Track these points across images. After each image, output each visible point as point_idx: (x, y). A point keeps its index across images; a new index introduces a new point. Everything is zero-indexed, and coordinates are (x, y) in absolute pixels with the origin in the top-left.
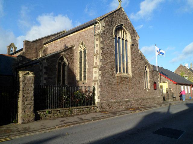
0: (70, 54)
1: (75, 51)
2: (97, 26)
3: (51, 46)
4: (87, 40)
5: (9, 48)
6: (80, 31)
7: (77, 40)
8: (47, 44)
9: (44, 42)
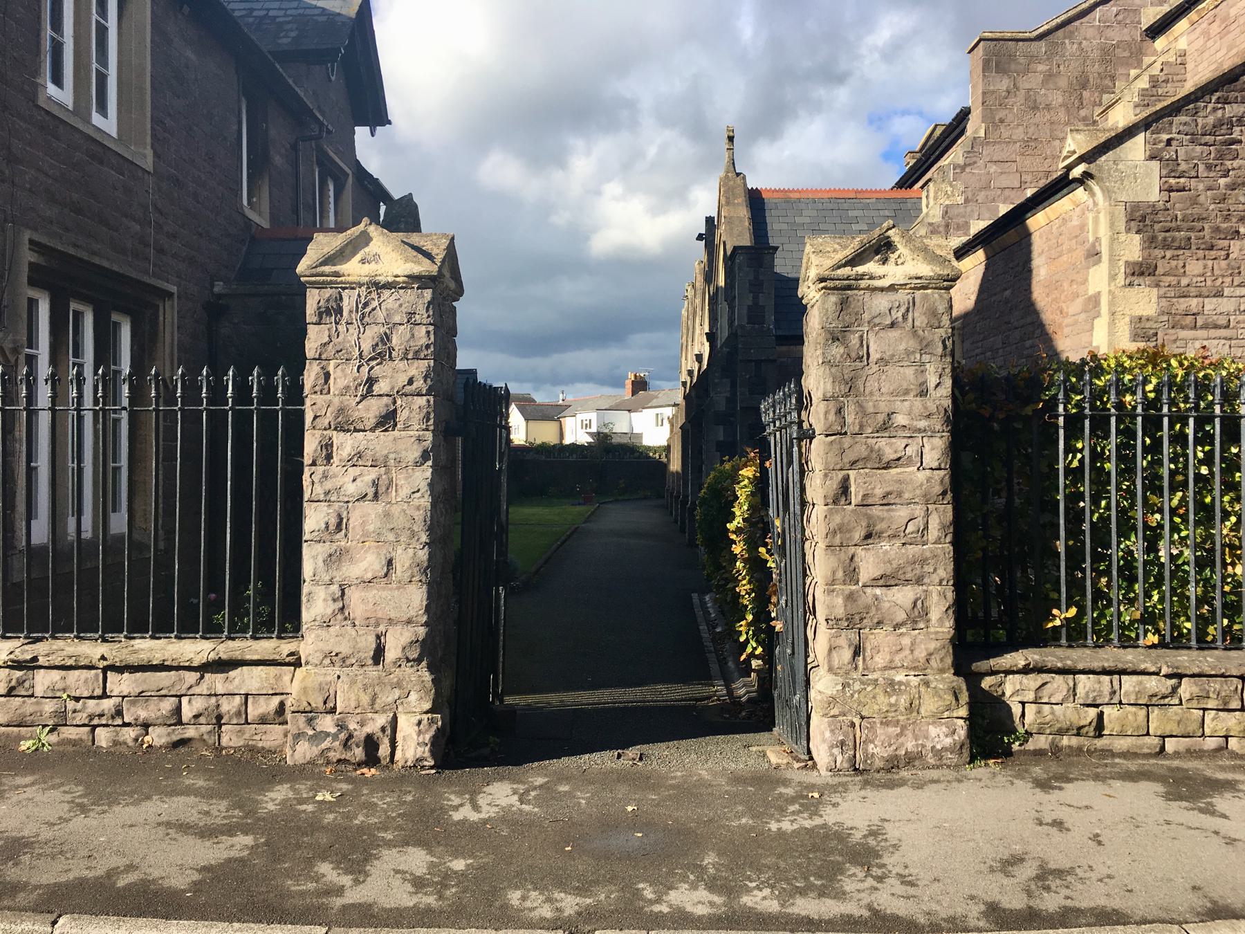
3: (1215, 28)
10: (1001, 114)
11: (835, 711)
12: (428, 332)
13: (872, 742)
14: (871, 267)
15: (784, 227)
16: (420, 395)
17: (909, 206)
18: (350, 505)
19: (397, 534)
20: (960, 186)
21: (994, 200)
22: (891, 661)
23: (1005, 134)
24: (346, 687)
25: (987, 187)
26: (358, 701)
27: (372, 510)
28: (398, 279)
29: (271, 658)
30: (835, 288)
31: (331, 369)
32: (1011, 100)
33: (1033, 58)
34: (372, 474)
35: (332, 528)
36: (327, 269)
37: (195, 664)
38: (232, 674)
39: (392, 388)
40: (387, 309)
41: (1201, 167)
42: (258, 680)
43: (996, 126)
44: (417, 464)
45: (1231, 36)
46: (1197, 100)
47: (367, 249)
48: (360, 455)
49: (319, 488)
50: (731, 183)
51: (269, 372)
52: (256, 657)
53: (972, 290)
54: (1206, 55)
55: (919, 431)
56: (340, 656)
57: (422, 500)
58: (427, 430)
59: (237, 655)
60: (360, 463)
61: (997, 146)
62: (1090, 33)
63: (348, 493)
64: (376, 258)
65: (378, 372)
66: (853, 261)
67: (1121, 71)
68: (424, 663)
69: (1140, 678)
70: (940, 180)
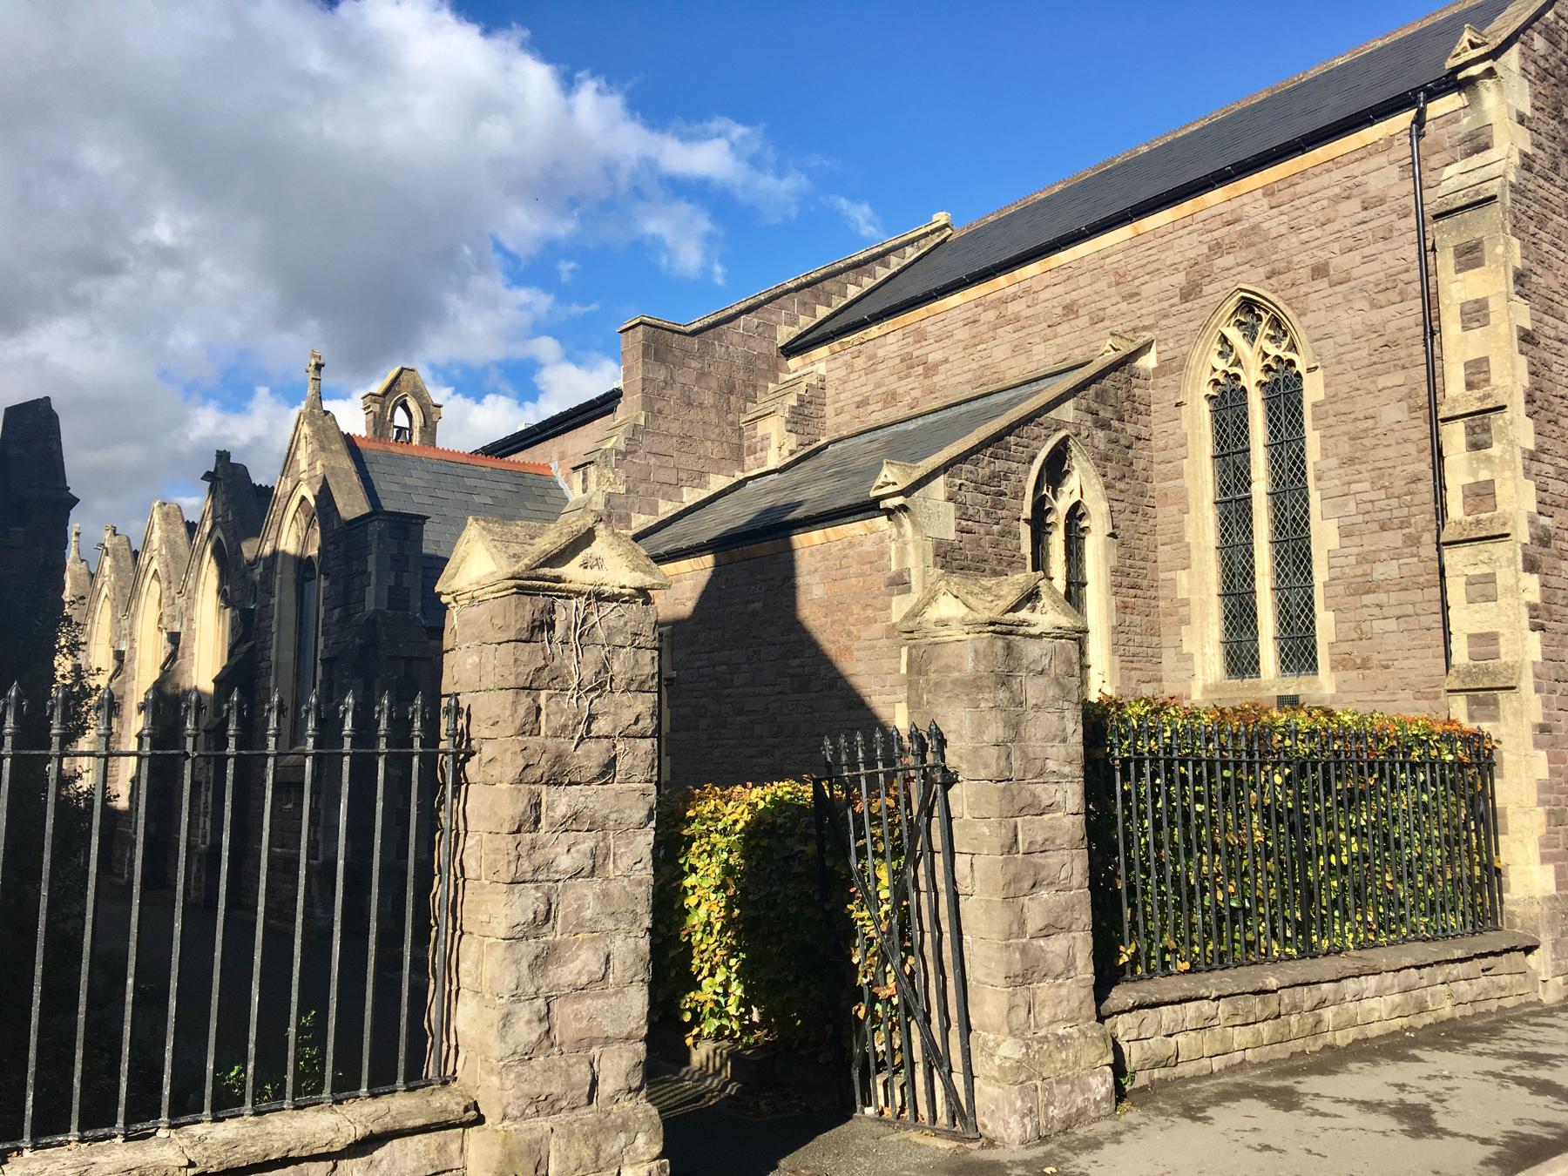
0: (1121, 420)
1: (1159, 395)
2: (1451, 118)
3: (860, 363)
4: (1319, 271)
5: (383, 408)
6: (1214, 197)
7: (1180, 279)
8: (822, 351)
9: (785, 334)
10: (659, 405)
11: (1023, 1077)
12: (653, 658)
13: (1052, 1104)
14: (1024, 614)
15: (395, 488)
16: (643, 737)
17: (529, 482)
18: (560, 884)
19: (617, 920)
20: (622, 473)
21: (653, 494)
22: (1055, 1014)
23: (663, 427)
24: (562, 1142)
25: (646, 480)
26: (580, 1159)
27: (588, 890)
28: (623, 591)
29: (442, 1119)
30: (1001, 633)
31: (542, 701)
32: (668, 392)
33: (687, 353)
34: (588, 842)
35: (540, 918)
36: (546, 571)
37: (337, 1147)
38: (378, 1154)
39: (614, 729)
40: (609, 627)
41: (982, 513)
42: (415, 1156)
43: (655, 417)
44: (642, 826)
45: (879, 375)
46: (977, 452)
47: (588, 551)
48: (576, 816)
49: (527, 864)
50: (320, 422)
51: (402, 700)
52: (420, 1122)
53: (688, 594)
54: (850, 385)
55: (1065, 776)
56: (550, 1099)
57: (644, 872)
58: (650, 781)
59: (389, 1123)
60: (574, 827)
61: (656, 438)
62: (736, 339)
63: (561, 868)
64: (598, 563)
65: (599, 707)
66: (1015, 608)
67: (761, 382)
68: (643, 1093)
69: (1197, 1003)
70: (602, 465)
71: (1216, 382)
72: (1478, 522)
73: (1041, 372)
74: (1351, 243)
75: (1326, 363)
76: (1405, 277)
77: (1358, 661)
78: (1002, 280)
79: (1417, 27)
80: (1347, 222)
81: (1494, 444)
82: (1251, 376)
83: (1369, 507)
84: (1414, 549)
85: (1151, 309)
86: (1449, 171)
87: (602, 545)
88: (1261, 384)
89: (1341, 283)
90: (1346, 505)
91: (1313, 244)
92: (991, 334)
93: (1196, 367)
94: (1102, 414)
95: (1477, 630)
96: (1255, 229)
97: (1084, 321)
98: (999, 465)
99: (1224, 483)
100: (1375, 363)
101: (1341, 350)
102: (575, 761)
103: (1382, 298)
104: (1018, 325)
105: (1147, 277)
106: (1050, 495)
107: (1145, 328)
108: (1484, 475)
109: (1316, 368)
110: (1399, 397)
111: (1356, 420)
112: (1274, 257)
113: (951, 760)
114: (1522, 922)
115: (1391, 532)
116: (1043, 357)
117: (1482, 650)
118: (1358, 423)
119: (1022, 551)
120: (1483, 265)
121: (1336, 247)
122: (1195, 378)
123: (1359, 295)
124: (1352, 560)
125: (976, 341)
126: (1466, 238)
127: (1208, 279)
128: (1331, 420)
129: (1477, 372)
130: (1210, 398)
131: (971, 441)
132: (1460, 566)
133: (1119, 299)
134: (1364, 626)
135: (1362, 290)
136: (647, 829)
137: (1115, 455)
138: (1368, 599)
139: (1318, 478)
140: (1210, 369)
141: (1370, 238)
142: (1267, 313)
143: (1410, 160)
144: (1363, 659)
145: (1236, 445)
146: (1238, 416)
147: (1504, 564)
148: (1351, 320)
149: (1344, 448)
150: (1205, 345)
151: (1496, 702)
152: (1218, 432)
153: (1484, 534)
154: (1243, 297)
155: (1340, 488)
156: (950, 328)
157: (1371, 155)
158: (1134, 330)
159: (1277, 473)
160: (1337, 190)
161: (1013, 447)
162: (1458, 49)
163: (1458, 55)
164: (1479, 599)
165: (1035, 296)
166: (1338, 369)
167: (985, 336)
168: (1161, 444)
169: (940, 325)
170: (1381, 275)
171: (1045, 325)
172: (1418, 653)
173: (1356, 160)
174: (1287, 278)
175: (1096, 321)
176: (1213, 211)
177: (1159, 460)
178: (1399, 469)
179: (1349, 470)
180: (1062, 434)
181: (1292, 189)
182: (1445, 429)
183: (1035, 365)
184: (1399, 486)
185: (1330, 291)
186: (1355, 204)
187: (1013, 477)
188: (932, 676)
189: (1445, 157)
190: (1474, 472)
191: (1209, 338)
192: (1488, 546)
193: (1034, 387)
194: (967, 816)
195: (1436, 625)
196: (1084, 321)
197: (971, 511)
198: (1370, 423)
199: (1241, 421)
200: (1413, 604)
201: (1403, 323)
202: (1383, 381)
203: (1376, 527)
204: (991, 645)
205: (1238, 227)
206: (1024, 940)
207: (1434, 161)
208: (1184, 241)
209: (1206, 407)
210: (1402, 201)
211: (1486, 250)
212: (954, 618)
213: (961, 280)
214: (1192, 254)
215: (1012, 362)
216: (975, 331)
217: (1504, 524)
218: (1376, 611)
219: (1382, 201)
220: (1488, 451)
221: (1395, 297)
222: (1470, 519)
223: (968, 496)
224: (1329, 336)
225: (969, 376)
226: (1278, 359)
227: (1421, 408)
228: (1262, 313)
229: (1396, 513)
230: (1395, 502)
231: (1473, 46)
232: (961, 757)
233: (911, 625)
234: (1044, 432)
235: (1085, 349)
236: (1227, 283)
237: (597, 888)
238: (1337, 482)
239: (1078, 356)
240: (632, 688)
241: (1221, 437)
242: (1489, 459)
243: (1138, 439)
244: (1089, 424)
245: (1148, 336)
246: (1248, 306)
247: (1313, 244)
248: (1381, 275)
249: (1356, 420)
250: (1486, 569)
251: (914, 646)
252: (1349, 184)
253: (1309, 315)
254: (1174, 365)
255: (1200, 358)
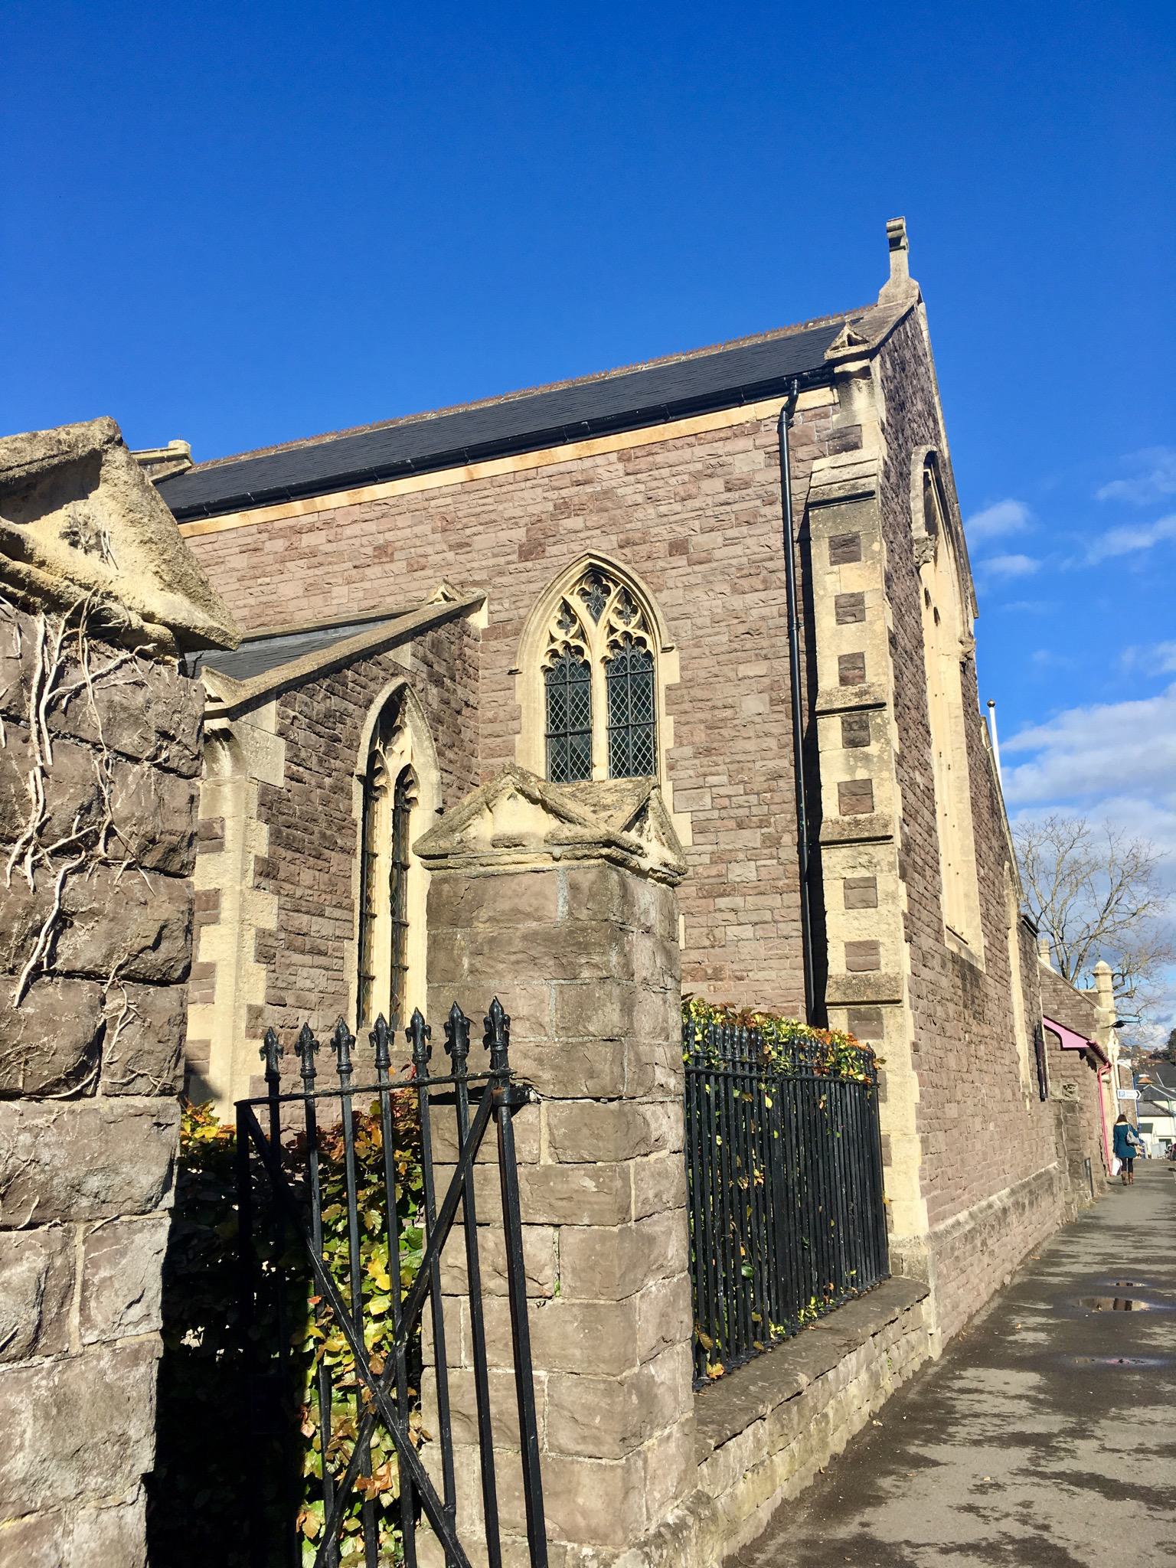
0: (453, 679)
1: (488, 658)
2: (821, 413)
4: (678, 547)
6: (565, 452)
7: (519, 534)
28: (149, 627)
39: (109, 956)
41: (314, 759)
57: (143, 1328)
65: (81, 896)
71: (554, 654)
72: (857, 823)
73: (343, 617)
74: (712, 522)
75: (684, 644)
76: (769, 565)
77: (710, 971)
78: (297, 506)
79: (721, 350)
80: (709, 500)
81: (873, 742)
82: (597, 650)
83: (726, 802)
84: (774, 850)
85: (484, 563)
86: (817, 465)
87: (111, 505)
88: (606, 661)
89: (701, 563)
90: (701, 799)
91: (673, 518)
92: (278, 566)
93: (534, 633)
94: (435, 666)
95: (855, 938)
96: (607, 493)
97: (400, 566)
98: (334, 702)
99: (558, 766)
100: (736, 650)
101: (700, 633)
102: (19, 1034)
103: (745, 583)
104: (315, 561)
105: (481, 528)
106: (381, 751)
107: (475, 583)
108: (861, 774)
109: (672, 648)
110: (761, 688)
111: (714, 708)
112: (628, 526)
113: (519, 1062)
114: (910, 1269)
115: (749, 830)
116: (344, 602)
117: (861, 960)
118: (716, 712)
119: (354, 815)
120: (859, 560)
121: (696, 525)
122: (532, 646)
123: (720, 578)
124: (706, 859)
125: (256, 572)
126: (842, 530)
127: (552, 540)
128: (687, 706)
129: (852, 667)
130: (547, 670)
131: (307, 664)
132: (839, 868)
133: (445, 547)
134: (717, 932)
135: (723, 573)
136: (158, 1213)
137: (446, 718)
138: (722, 902)
139: (671, 768)
140: (548, 637)
141: (733, 520)
142: (616, 584)
143: (777, 448)
144: (715, 969)
145: (573, 725)
146: (577, 693)
147: (886, 868)
148: (709, 603)
149: (700, 736)
150: (545, 610)
151: (879, 1017)
152: (553, 709)
153: (866, 835)
154: (591, 564)
155: (694, 780)
156: (220, 553)
157: (736, 436)
158: (462, 584)
159: (620, 759)
160: (699, 466)
161: (351, 685)
162: (838, 342)
163: (836, 348)
164: (859, 905)
165: (339, 530)
166: (696, 652)
167: (268, 569)
168: (490, 715)
169: (209, 547)
170: (745, 560)
171: (350, 565)
172: (774, 963)
173: (721, 439)
174: (643, 550)
175: (415, 567)
176: (562, 468)
177: (486, 733)
178: (759, 764)
179: (705, 761)
180: (400, 680)
181: (650, 458)
182: (822, 722)
183: (333, 610)
184: (759, 783)
185: (689, 570)
186: (718, 484)
187: (348, 720)
188: (480, 927)
189: (814, 449)
190: (851, 770)
191: (550, 603)
192: (869, 848)
193: (332, 634)
194: (547, 1160)
195: (795, 934)
196: (400, 566)
197: (303, 754)
198: (728, 713)
199: (581, 699)
200: (772, 910)
201: (766, 611)
202: (744, 670)
203: (732, 824)
204: (603, 877)
205: (589, 489)
206: (636, 1370)
207: (802, 452)
208: (526, 494)
209: (541, 679)
210: (769, 488)
211: (862, 545)
212: (534, 835)
213: (245, 497)
214: (535, 509)
215: (304, 603)
216: (255, 560)
217: (886, 826)
218: (731, 916)
219: (746, 485)
220: (866, 749)
221: (757, 583)
222: (847, 818)
223: (300, 735)
224: (686, 616)
225: (245, 612)
226: (627, 636)
227: (783, 701)
228: (611, 585)
229: (755, 811)
230: (753, 799)
231: (851, 342)
232: (540, 1061)
233: (445, 844)
234: (382, 674)
235: (400, 598)
236: (575, 547)
237: (42, 1386)
238: (691, 772)
239: (390, 604)
240: (149, 861)
241: (557, 715)
242: (867, 758)
243: (467, 705)
244: (424, 676)
245: (478, 592)
246: (597, 576)
247: (673, 518)
248: (745, 560)
249: (714, 708)
250: (867, 874)
251: (445, 880)
252: (713, 462)
253: (665, 591)
254: (509, 628)
255: (539, 624)
